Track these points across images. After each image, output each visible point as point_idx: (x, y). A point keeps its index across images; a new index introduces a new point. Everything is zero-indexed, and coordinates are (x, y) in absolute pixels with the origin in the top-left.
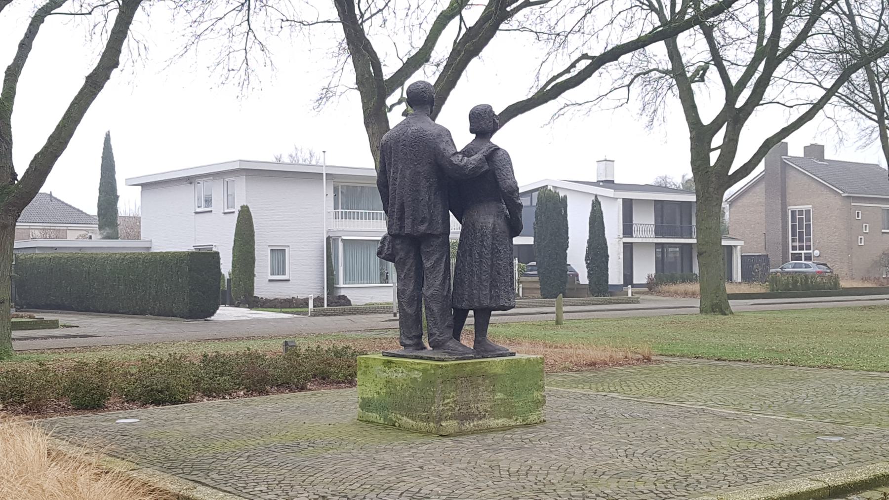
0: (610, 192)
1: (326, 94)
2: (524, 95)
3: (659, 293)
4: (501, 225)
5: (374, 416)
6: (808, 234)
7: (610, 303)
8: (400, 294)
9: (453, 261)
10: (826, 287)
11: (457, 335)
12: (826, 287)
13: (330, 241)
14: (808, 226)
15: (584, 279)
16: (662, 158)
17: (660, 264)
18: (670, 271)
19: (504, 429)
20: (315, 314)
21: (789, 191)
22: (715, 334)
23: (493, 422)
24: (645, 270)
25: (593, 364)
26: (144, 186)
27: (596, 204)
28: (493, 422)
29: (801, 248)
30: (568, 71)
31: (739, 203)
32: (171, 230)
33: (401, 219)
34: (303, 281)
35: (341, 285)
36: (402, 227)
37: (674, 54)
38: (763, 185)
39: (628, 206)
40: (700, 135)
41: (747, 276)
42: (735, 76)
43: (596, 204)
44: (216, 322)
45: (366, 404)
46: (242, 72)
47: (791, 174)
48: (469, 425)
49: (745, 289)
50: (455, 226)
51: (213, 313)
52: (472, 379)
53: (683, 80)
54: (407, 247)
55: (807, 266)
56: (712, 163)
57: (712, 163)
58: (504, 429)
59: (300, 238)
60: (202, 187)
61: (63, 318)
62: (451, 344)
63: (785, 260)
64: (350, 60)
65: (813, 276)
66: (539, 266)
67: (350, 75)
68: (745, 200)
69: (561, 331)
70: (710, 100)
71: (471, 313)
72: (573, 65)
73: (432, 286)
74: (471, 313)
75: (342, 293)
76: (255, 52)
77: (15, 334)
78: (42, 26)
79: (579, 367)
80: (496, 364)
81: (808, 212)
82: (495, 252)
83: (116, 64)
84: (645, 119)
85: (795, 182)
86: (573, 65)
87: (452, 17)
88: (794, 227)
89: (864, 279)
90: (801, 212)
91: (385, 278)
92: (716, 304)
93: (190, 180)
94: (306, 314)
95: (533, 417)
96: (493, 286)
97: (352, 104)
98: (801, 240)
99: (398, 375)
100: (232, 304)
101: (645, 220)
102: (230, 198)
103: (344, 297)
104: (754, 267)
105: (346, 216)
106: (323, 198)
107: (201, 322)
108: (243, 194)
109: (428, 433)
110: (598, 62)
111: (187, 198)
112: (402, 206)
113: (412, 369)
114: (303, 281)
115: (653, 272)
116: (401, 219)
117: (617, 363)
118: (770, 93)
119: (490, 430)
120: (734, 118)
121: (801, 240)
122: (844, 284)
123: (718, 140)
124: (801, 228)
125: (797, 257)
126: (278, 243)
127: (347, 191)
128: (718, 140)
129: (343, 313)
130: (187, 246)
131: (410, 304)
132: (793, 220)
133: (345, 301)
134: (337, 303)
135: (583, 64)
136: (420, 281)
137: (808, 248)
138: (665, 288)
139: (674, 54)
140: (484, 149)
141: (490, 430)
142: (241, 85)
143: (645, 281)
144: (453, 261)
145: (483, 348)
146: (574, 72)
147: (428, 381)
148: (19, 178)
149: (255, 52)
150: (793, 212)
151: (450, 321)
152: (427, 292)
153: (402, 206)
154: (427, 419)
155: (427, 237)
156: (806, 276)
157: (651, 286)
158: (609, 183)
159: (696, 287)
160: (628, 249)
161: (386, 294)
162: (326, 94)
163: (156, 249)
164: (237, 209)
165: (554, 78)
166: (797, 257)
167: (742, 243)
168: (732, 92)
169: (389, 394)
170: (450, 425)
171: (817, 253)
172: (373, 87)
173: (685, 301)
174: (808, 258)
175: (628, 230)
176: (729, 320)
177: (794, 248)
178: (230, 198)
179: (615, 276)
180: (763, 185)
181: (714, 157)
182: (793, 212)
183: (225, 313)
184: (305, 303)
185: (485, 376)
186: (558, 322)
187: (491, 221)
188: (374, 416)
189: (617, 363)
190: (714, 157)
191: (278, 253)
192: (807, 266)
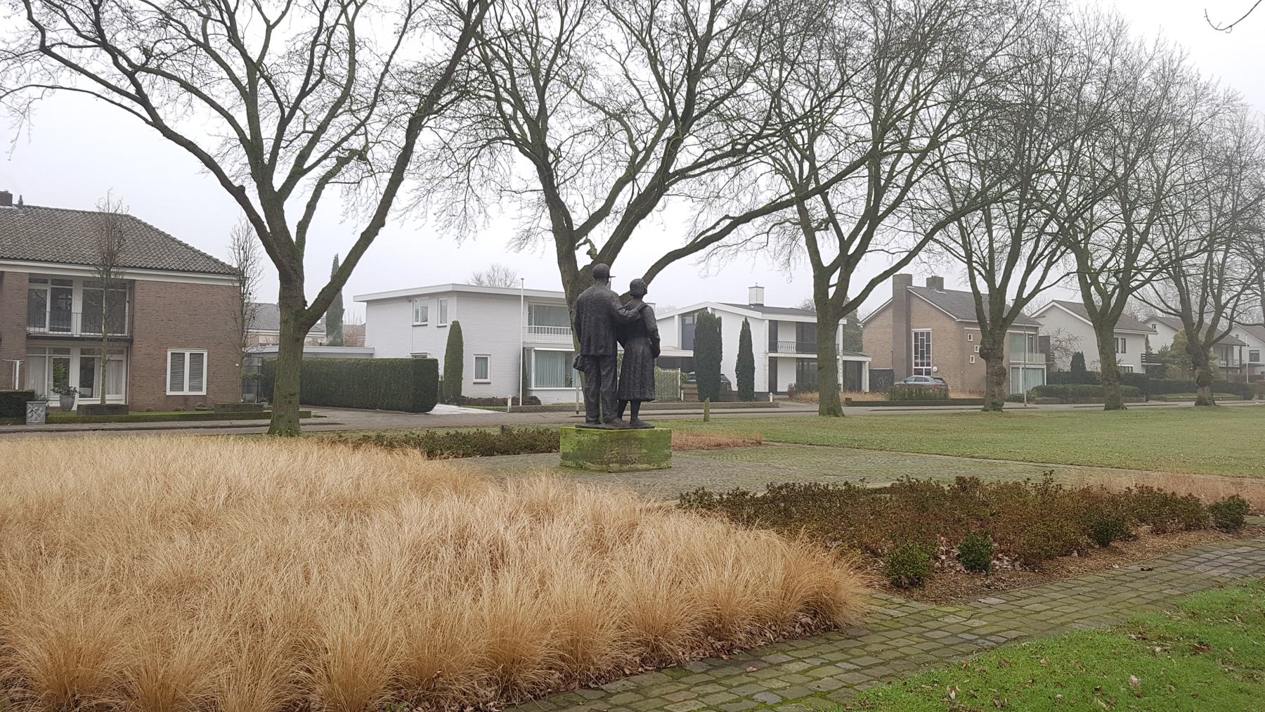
0: (758, 315)
1: (527, 235)
2: (681, 245)
3: (798, 400)
4: (647, 351)
5: (569, 463)
6: (928, 352)
7: (754, 407)
8: (586, 391)
9: (619, 370)
10: (938, 398)
11: (620, 415)
12: (938, 398)
13: (526, 351)
14: (928, 346)
15: (735, 388)
16: (793, 288)
17: (801, 375)
18: (804, 385)
19: (647, 470)
20: (512, 411)
21: (913, 315)
22: (832, 428)
23: (640, 466)
24: (786, 380)
25: (719, 445)
26: (370, 303)
27: (746, 325)
28: (640, 466)
29: (922, 365)
30: (713, 227)
31: (872, 325)
32: (391, 341)
33: (589, 346)
34: (502, 383)
35: (533, 388)
36: (589, 351)
37: (803, 212)
38: (890, 313)
39: (774, 326)
40: (822, 274)
41: (873, 388)
42: (847, 230)
43: (746, 325)
44: (434, 416)
45: (565, 456)
46: (461, 218)
47: (915, 302)
48: (626, 467)
49: (869, 398)
50: (620, 347)
51: (431, 409)
52: (627, 440)
53: (808, 227)
54: (591, 361)
55: (926, 380)
56: (830, 296)
57: (830, 296)
58: (647, 470)
59: (500, 351)
60: (419, 304)
61: (314, 412)
62: (616, 420)
63: (909, 374)
64: (547, 211)
65: (929, 387)
66: (697, 375)
67: (546, 222)
68: (876, 323)
69: (706, 426)
70: (829, 250)
71: (629, 404)
72: (718, 223)
73: (606, 386)
74: (629, 404)
75: (534, 394)
76: (473, 203)
77: (301, 421)
78: (323, 192)
79: (709, 447)
80: (642, 433)
81: (928, 334)
82: (643, 366)
83: (383, 225)
84: (782, 259)
85: (918, 308)
86: (718, 223)
87: (627, 182)
88: (916, 346)
89: (963, 391)
90: (922, 334)
91: (569, 383)
92: (831, 409)
93: (409, 299)
94: (505, 410)
95: (664, 465)
96: (642, 387)
97: (548, 246)
98: (922, 358)
99: (584, 438)
100: (443, 402)
101: (788, 339)
102: (443, 312)
103: (535, 398)
104: (881, 379)
105: (537, 331)
106: (521, 315)
107: (422, 415)
108: (454, 312)
109: (602, 471)
110: (736, 222)
111: (406, 314)
112: (589, 340)
113: (593, 435)
114: (502, 383)
115: (794, 381)
116: (589, 346)
117: (736, 445)
118: (877, 238)
119: (638, 470)
120: (847, 262)
121: (922, 358)
122: (952, 396)
123: (834, 279)
124: (923, 348)
125: (919, 372)
126: (482, 352)
127: (540, 310)
128: (834, 279)
129: (535, 411)
130: (404, 353)
131: (593, 395)
132: (916, 340)
133: (536, 401)
134: (531, 403)
135: (728, 222)
136: (599, 384)
137: (928, 364)
138: (803, 396)
139: (803, 212)
140: (639, 306)
141: (638, 470)
142: (460, 228)
143: (786, 390)
144: (619, 370)
145: (635, 423)
146: (718, 229)
147: (602, 441)
148: (309, 305)
149: (473, 203)
150: (916, 334)
151: (616, 407)
152: (603, 389)
153: (589, 340)
154: (602, 463)
155: (603, 357)
156: (920, 388)
157: (792, 394)
158: (759, 307)
159: (817, 395)
160: (773, 363)
161: (574, 396)
162: (527, 235)
163: (378, 356)
164: (449, 324)
165: (704, 233)
166: (919, 372)
167: (870, 359)
168: (844, 245)
169: (579, 449)
170: (615, 466)
171: (935, 369)
172: (567, 236)
173: (809, 407)
174: (928, 373)
175: (773, 346)
176: (839, 420)
177: (916, 364)
178: (443, 312)
179: (761, 384)
180: (890, 313)
181: (832, 291)
182: (916, 334)
183: (440, 409)
184: (505, 402)
185: (636, 439)
186: (705, 420)
187: (641, 348)
188: (569, 463)
189: (736, 445)
190: (832, 291)
191: (482, 361)
192: (926, 380)
